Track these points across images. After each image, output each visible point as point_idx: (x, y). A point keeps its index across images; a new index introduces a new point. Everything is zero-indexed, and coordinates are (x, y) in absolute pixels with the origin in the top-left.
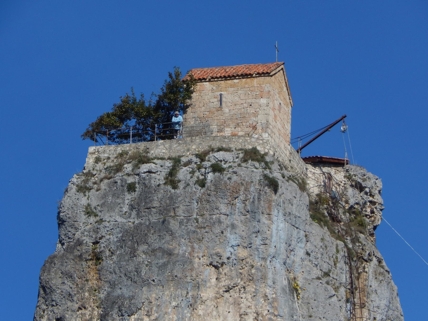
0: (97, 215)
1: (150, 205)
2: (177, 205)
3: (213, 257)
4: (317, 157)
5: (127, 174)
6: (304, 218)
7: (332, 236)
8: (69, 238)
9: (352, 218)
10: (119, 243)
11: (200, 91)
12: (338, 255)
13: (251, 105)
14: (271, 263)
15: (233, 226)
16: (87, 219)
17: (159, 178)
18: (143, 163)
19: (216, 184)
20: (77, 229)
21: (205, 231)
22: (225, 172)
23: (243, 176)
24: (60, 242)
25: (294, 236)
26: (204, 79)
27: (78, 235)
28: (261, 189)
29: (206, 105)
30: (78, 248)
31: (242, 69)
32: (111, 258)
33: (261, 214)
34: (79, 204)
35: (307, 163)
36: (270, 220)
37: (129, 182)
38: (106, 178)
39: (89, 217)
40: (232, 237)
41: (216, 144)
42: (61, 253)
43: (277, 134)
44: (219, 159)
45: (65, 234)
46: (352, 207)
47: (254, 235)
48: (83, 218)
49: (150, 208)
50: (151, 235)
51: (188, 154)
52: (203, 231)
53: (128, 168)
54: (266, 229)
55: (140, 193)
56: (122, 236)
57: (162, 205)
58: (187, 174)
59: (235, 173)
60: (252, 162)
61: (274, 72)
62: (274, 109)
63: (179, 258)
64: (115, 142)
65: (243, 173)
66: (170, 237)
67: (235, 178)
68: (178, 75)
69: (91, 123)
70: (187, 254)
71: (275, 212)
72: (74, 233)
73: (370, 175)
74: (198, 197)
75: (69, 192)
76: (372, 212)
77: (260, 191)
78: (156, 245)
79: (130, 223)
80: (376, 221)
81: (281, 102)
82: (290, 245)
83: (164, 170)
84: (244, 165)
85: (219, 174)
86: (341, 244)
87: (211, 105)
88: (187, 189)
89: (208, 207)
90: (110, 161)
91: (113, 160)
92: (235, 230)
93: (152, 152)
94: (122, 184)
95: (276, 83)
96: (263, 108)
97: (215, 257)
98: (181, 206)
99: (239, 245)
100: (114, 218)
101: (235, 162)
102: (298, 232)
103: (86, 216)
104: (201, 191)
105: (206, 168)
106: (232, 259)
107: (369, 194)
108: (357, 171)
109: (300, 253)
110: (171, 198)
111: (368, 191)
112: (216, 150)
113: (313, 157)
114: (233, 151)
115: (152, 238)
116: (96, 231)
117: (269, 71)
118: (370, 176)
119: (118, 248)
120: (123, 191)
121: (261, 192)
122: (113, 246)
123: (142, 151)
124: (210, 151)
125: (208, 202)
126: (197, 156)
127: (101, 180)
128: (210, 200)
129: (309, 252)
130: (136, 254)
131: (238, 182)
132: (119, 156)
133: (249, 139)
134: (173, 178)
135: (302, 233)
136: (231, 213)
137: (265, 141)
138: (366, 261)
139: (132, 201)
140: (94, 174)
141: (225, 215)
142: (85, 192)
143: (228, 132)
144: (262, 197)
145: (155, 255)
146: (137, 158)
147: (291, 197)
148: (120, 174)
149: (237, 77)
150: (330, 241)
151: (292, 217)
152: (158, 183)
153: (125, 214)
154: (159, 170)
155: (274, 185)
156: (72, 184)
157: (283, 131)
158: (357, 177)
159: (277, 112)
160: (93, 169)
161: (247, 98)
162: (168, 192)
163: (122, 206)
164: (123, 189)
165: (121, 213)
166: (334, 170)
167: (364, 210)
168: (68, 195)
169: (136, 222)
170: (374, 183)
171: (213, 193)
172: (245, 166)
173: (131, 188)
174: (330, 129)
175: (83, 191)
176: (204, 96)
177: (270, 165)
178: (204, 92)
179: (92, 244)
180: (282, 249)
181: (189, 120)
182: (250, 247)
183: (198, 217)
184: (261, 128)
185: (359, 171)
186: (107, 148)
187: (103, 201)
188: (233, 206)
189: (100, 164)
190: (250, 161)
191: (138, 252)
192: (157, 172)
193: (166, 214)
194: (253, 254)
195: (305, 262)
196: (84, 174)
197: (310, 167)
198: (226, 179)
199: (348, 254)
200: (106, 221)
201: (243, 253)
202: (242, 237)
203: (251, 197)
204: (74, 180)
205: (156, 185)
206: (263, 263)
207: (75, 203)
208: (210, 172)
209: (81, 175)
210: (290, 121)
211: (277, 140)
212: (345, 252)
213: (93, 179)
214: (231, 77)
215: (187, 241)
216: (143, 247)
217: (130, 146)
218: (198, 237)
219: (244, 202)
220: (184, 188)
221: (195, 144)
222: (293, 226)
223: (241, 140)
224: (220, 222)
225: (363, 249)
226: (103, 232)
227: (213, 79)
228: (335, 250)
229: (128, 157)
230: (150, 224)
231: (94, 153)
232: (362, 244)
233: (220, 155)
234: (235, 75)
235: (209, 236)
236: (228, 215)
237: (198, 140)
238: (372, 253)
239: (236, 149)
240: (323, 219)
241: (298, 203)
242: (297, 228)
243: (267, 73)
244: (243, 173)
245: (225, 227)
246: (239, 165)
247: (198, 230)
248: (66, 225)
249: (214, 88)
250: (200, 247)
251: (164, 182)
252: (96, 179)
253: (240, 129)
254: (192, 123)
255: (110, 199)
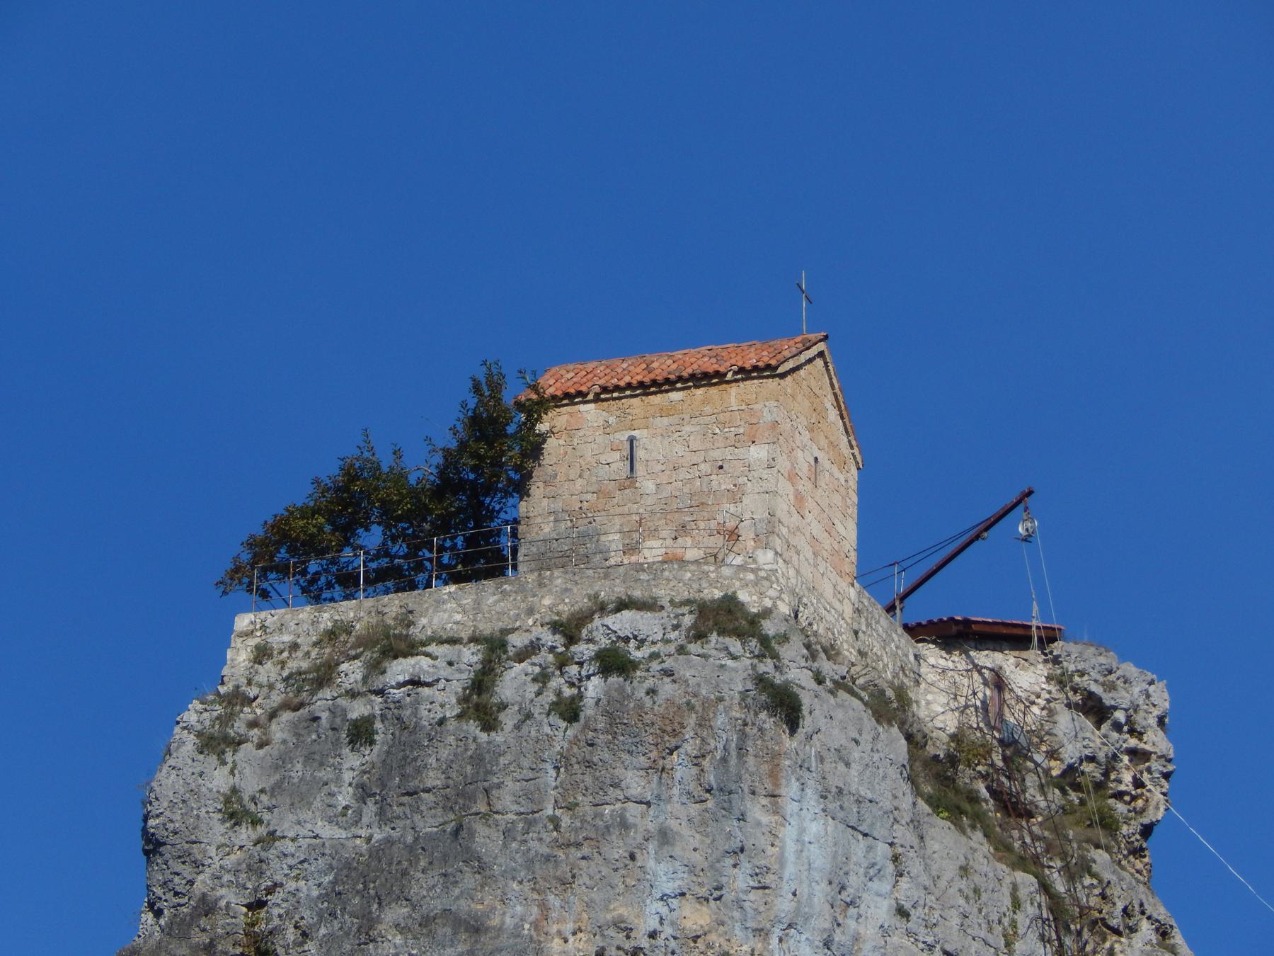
0: (261, 822)
1: (416, 782)
2: (496, 781)
3: (606, 933)
4: (952, 619)
5: (347, 692)
6: (888, 803)
7: (1000, 860)
8: (176, 894)
9: (1071, 802)
10: (326, 904)
11: (570, 431)
12: (1020, 917)
13: (721, 467)
14: (785, 946)
15: (665, 837)
16: (231, 834)
17: (444, 700)
18: (396, 657)
19: (613, 711)
20: (198, 865)
21: (579, 855)
22: (638, 673)
23: (692, 681)
24: (151, 906)
25: (854, 859)
26: (580, 394)
27: (203, 882)
28: (748, 720)
29: (586, 474)
30: (203, 922)
31: (698, 359)
32: (300, 950)
33: (748, 797)
34: (204, 790)
35: (918, 641)
36: (776, 813)
37: (354, 715)
38: (286, 706)
39: (237, 828)
40: (662, 868)
41: (610, 590)
42: (152, 942)
43: (807, 552)
44: (620, 634)
45: (165, 883)
46: (1071, 770)
47: (729, 861)
48: (217, 830)
49: (416, 793)
50: (419, 875)
51: (530, 622)
52: (575, 853)
53: (352, 672)
54: (763, 842)
55: (386, 748)
56: (335, 882)
57: (451, 782)
58: (525, 684)
59: (668, 673)
60: (721, 639)
61: (790, 365)
62: (792, 477)
63: (504, 940)
64: (325, 600)
65: (693, 672)
66: (477, 876)
67: (667, 688)
68: (495, 386)
69: (245, 539)
70: (527, 926)
71: (790, 789)
72: (189, 878)
73: (1130, 669)
74: (559, 753)
75: (175, 755)
76: (1138, 783)
77: (746, 724)
78: (435, 905)
79: (358, 841)
80: (1151, 810)
81: (820, 455)
82: (843, 888)
83: (457, 676)
84: (694, 648)
85: (621, 679)
86: (1027, 882)
87: (603, 472)
88: (525, 729)
89: (588, 780)
90: (300, 654)
91: (308, 654)
92: (670, 848)
93: (424, 621)
94: (333, 722)
95: (799, 398)
96: (756, 474)
97: (611, 932)
98: (509, 782)
99: (683, 894)
100: (309, 826)
101: (668, 641)
102: (870, 848)
103: (228, 825)
104: (568, 733)
105: (581, 664)
106: (663, 936)
107: (1126, 728)
108: (1085, 660)
109: (878, 909)
110: (477, 759)
111: (1123, 720)
112: (611, 606)
113: (941, 620)
114: (662, 608)
115: (424, 884)
116: (257, 868)
117: (773, 362)
118: (1128, 675)
119: (321, 917)
120: (336, 744)
121: (747, 729)
122: (307, 914)
123: (395, 619)
124: (593, 614)
125: (589, 765)
126: (556, 627)
127: (273, 715)
128: (595, 759)
129: (907, 906)
130: (374, 933)
131: (678, 701)
132: (326, 640)
133: (712, 568)
134: (485, 696)
135: (882, 850)
136: (658, 797)
137: (762, 574)
138: (1117, 932)
139: (365, 772)
140: (252, 696)
141: (641, 803)
142: (223, 752)
143: (653, 551)
144: (750, 743)
145: (431, 935)
146: (377, 642)
147: (843, 742)
148: (327, 693)
149: (679, 385)
150: (991, 875)
151: (848, 802)
152: (439, 716)
153: (344, 815)
154: (444, 675)
155: (786, 707)
156: (184, 728)
157: (827, 542)
158: (1086, 677)
159: (805, 486)
160: (249, 683)
161: (709, 445)
162: (470, 741)
163: (334, 789)
164: (337, 740)
165: (330, 812)
166: (1012, 660)
167: (1113, 777)
168: (172, 762)
169: (377, 837)
170: (1143, 693)
171: (602, 738)
172: (700, 651)
173: (361, 733)
174: (985, 534)
175: (219, 749)
176: (580, 445)
177: (777, 647)
178: (581, 433)
179: (245, 910)
180: (816, 900)
181: (539, 520)
182: (719, 898)
183: (558, 812)
184: (752, 536)
185: (1093, 661)
186: (288, 616)
187: (277, 777)
188: (664, 775)
189: (269, 665)
190: (714, 637)
191: (380, 927)
192: (438, 680)
193: (463, 808)
194: (726, 919)
195: (895, 939)
196: (221, 698)
197: (933, 655)
198: (643, 695)
199: (1051, 910)
200: (284, 837)
201: (695, 917)
202: (692, 869)
203: (716, 745)
204: (191, 717)
205: (433, 722)
206: (760, 945)
207: (193, 786)
208: (593, 675)
209: (213, 702)
210: (853, 511)
211: (807, 571)
212: (1040, 906)
213: (247, 713)
214: (660, 385)
215: (526, 889)
216: (396, 913)
217: (360, 607)
218: (558, 873)
219: (697, 760)
220: (517, 727)
221: (550, 590)
222: (853, 828)
223: (689, 575)
224: (624, 825)
225: (1103, 896)
226: (277, 870)
227: (605, 393)
228: (1007, 901)
229: (352, 639)
230: (416, 839)
231: (250, 634)
232: (1100, 881)
233: (623, 622)
234: (672, 377)
235: (593, 869)
236: (648, 804)
237: (559, 579)
238: (1137, 908)
239: (671, 602)
240: (967, 806)
241: (867, 760)
242: (866, 835)
243: (768, 367)
244: (693, 672)
245: (639, 839)
246: (681, 650)
247: (561, 854)
248: (167, 856)
249: (612, 420)
250: (566, 905)
251: (457, 711)
252: (259, 711)
253: (689, 540)
254: (547, 529)
255: (298, 770)
